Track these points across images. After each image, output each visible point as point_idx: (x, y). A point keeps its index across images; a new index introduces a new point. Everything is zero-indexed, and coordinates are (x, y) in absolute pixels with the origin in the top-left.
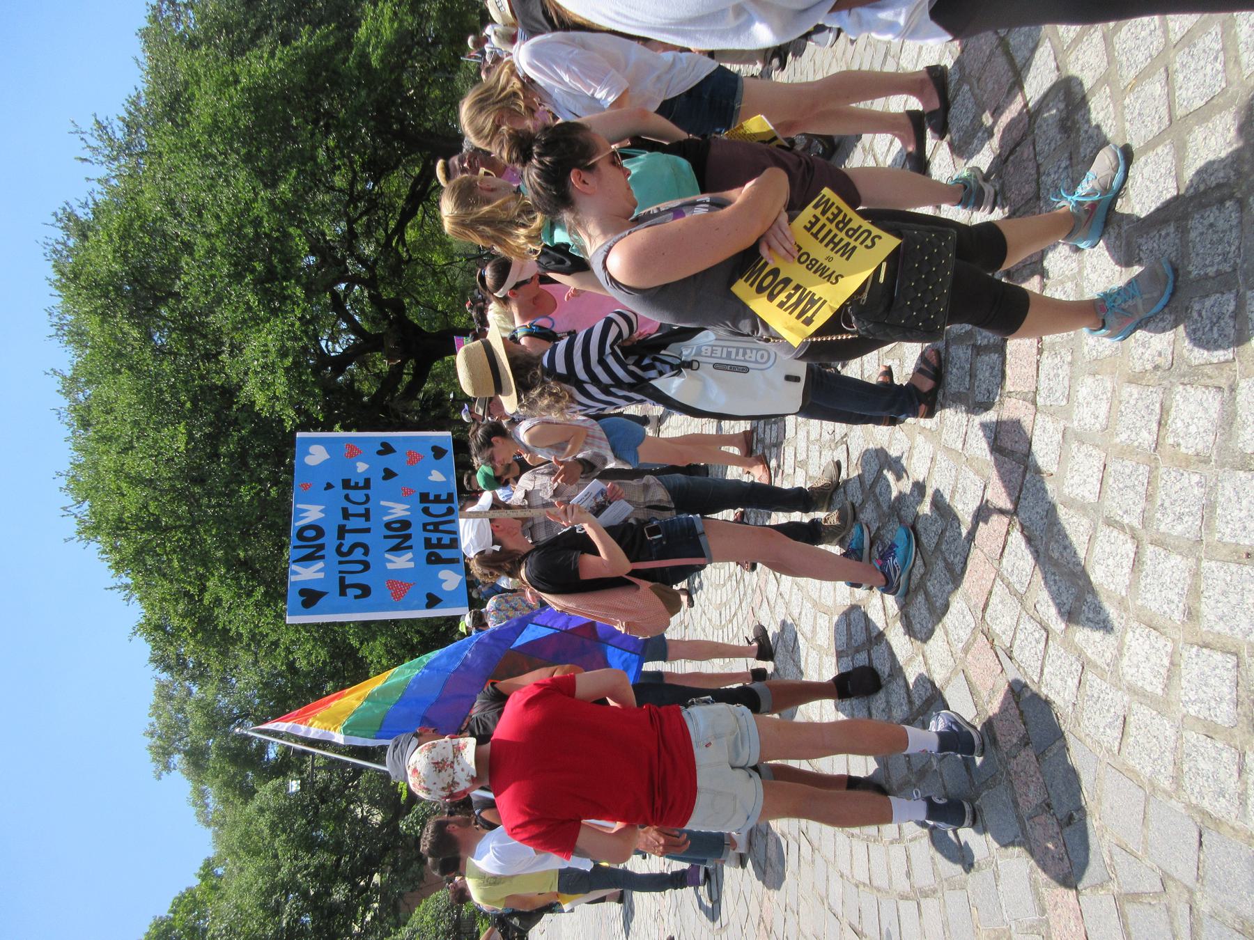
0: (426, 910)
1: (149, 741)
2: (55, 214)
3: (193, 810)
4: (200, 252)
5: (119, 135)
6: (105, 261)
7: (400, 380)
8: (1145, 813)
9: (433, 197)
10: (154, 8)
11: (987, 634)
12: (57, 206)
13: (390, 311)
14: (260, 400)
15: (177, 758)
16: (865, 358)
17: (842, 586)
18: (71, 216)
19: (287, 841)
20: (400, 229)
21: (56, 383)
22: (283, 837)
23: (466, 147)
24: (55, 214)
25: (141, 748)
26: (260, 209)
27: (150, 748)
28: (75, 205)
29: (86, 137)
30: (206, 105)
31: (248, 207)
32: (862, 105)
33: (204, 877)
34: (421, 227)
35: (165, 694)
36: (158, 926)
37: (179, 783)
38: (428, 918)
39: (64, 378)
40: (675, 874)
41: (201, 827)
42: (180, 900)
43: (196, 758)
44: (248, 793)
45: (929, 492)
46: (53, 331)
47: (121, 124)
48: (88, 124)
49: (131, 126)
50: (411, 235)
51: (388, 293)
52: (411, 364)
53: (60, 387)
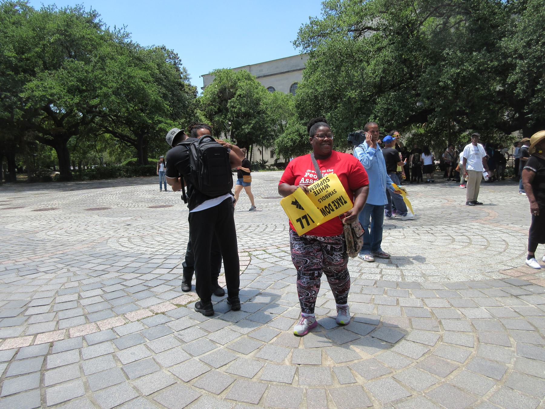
4: (86, 68)
5: (126, 40)
6: (77, 32)
7: (40, 132)
8: (27, 358)
11: (45, 360)
12: (99, 11)
13: (74, 128)
18: (95, 16)
20: (108, 131)
26: (105, 89)
28: (100, 18)
29: (123, 30)
30: (138, 73)
31: (106, 86)
32: (222, 270)
34: (111, 139)
39: (26, 3)
45: (293, 187)
46: (46, 6)
47: (129, 41)
48: (128, 30)
49: (129, 45)
50: (107, 135)
51: (81, 128)
52: (51, 138)
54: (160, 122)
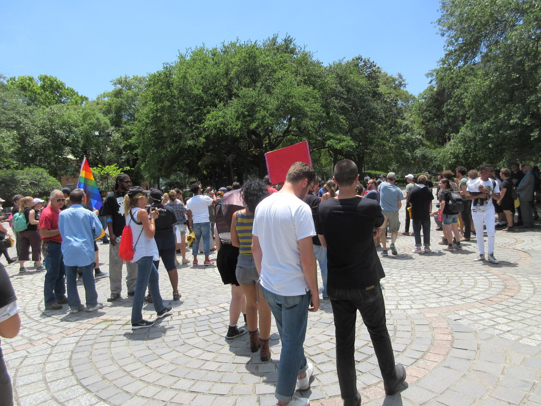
0: (54, 181)
1: (123, 76)
2: (289, 36)
3: (102, 93)
9: (122, 178)
10: (368, 60)
14: (209, 116)
15: (119, 86)
16: (373, 349)
17: (86, 302)
19: (87, 129)
21: (234, 40)
22: (88, 128)
23: (311, 170)
24: (289, 36)
25: (116, 76)
27: (121, 78)
28: (294, 42)
33: (81, 97)
35: (140, 81)
36: (62, 84)
37: (111, 89)
38: (50, 182)
40: (371, 328)
41: (97, 96)
42: (73, 91)
43: (118, 94)
44: (107, 112)
53: (233, 42)
54: (330, 138)
